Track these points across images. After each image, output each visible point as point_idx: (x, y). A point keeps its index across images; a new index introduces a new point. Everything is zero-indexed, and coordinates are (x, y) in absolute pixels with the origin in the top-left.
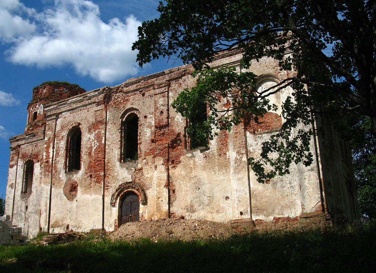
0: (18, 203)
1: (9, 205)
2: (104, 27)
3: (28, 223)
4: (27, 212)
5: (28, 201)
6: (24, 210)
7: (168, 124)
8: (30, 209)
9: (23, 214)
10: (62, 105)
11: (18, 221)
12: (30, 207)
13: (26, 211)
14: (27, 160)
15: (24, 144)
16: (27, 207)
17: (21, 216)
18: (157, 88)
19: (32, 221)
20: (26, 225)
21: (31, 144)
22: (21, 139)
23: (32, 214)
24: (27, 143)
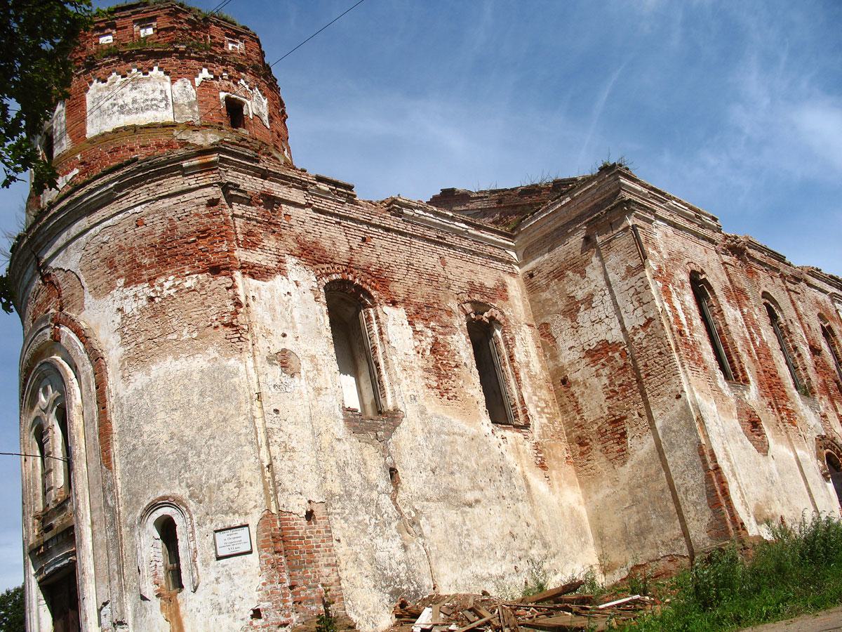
0: (339, 447)
1: (293, 450)
2: (776, 445)
3: (421, 540)
4: (402, 495)
5: (391, 448)
6: (383, 483)
7: (340, 577)
8: (412, 482)
9: (386, 501)
10: (731, 362)
11: (364, 531)
12: (410, 473)
13: (396, 490)
14: (334, 277)
15: (302, 207)
16: (393, 472)
17: (373, 509)
18: (250, 74)
19: (439, 534)
20: (412, 547)
21: (337, 223)
22: (285, 177)
23: (431, 504)
24: (316, 210)
